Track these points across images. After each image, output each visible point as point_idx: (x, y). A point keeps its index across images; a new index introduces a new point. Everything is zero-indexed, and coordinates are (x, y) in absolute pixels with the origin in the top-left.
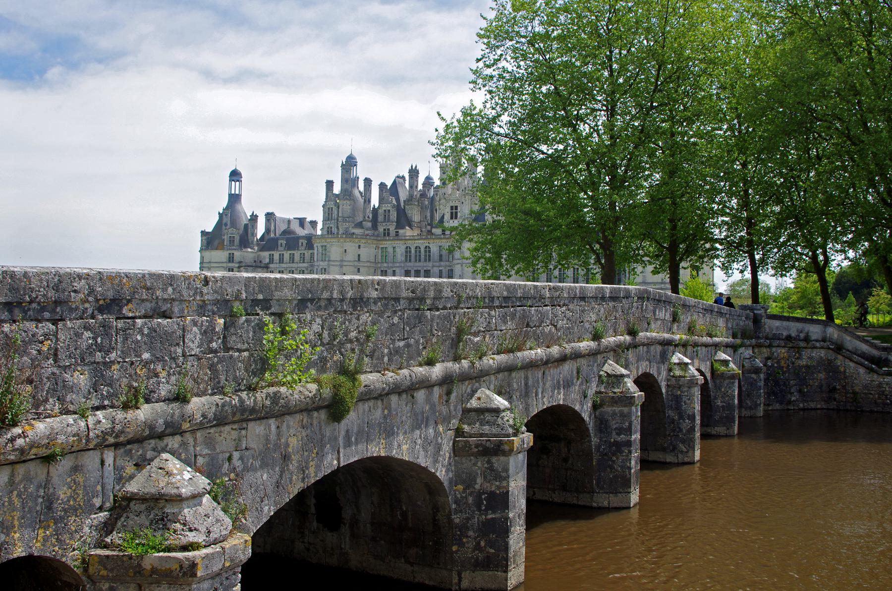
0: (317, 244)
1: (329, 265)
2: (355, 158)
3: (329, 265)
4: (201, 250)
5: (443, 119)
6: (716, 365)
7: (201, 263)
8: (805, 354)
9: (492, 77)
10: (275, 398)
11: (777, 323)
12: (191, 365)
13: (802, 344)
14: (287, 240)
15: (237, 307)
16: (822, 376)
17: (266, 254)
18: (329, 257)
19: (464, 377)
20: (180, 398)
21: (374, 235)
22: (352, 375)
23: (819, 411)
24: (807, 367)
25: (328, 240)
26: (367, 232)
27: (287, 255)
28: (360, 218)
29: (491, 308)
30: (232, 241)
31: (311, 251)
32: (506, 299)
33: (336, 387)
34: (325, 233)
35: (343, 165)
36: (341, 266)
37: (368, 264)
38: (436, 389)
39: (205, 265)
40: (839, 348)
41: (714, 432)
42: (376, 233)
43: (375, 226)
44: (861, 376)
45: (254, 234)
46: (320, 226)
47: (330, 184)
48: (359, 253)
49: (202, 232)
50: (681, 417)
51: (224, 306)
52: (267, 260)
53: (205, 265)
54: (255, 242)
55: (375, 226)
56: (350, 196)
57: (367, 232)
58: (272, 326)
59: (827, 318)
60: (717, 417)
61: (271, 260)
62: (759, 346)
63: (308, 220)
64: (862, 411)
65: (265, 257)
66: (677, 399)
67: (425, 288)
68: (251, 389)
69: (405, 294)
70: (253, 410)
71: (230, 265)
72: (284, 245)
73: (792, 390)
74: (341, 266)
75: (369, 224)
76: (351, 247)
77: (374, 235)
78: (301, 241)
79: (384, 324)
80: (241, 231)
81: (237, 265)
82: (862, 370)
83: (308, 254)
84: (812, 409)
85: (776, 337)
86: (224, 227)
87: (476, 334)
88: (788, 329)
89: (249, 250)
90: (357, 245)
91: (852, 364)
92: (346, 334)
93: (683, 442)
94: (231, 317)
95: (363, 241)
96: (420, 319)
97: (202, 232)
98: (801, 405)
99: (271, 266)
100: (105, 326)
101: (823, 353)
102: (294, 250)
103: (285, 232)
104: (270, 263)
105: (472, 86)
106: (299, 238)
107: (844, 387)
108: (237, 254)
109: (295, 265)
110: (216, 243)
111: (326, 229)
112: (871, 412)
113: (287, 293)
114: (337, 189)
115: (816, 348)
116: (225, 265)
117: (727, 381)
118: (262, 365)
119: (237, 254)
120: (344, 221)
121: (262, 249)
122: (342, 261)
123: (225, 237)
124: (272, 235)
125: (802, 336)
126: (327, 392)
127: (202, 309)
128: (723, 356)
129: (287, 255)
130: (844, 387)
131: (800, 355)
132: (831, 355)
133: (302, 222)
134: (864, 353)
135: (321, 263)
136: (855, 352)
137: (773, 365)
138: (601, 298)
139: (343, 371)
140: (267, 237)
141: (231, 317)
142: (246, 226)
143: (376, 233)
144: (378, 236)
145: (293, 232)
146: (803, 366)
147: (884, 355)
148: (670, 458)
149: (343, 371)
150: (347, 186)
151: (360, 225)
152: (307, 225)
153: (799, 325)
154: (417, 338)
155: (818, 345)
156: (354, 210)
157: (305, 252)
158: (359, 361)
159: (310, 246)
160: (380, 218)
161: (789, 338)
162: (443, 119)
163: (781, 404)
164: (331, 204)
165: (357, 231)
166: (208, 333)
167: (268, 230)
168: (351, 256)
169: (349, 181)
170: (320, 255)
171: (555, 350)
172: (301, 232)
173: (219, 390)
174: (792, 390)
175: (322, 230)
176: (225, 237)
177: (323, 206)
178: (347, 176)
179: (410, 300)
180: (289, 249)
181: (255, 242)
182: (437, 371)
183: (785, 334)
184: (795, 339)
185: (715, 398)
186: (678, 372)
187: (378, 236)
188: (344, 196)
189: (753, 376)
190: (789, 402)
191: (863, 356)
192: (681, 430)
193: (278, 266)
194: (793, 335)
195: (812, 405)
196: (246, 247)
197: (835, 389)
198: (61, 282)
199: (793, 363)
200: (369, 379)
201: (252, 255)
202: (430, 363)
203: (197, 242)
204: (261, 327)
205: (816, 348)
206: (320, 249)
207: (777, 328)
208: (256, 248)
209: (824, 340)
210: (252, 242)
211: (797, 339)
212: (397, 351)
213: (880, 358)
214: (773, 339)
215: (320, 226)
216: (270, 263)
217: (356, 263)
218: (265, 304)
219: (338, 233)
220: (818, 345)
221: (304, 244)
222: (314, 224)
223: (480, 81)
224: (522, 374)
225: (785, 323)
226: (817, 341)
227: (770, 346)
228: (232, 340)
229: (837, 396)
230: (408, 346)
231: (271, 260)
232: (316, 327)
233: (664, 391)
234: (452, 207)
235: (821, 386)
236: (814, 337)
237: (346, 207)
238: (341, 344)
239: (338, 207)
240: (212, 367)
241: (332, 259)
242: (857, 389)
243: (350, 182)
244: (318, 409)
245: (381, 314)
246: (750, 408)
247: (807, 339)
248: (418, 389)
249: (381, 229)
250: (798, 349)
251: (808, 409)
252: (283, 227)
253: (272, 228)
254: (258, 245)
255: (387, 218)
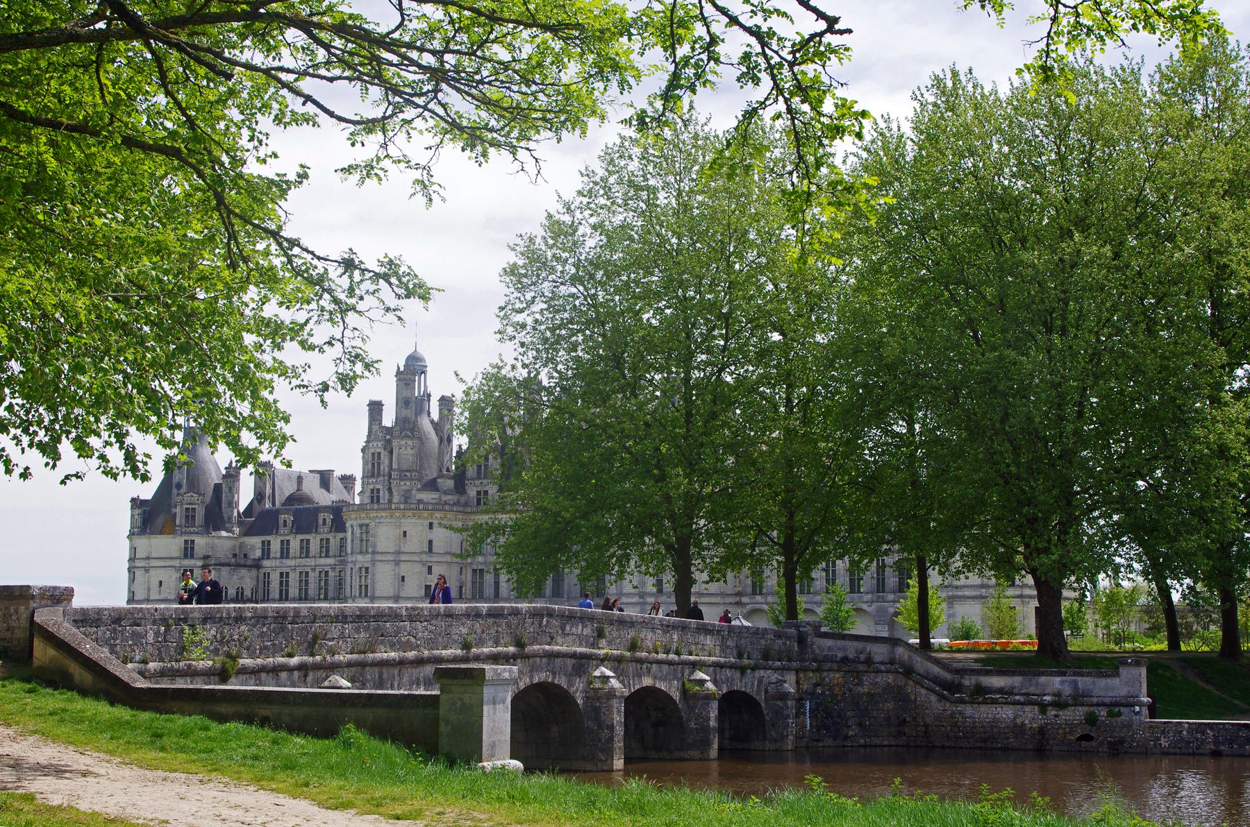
0: (351, 522)
1: (373, 562)
2: (420, 359)
3: (373, 562)
4: (131, 535)
5: (462, 380)
6: (688, 685)
7: (131, 560)
8: (867, 679)
9: (523, 326)
10: (189, 666)
11: (829, 643)
12: (150, 648)
13: (862, 668)
14: (297, 514)
15: (171, 621)
16: (890, 706)
17: (255, 541)
18: (374, 546)
19: (316, 667)
20: (145, 662)
21: (457, 503)
22: (234, 659)
23: (886, 749)
24: (869, 695)
25: (373, 514)
26: (444, 498)
27: (295, 544)
28: (431, 473)
29: (345, 623)
30: (190, 516)
31: (340, 535)
32: (358, 616)
33: (224, 664)
34: (367, 501)
35: (399, 373)
36: (397, 563)
37: (448, 558)
38: (296, 674)
39: (138, 564)
40: (908, 671)
41: (686, 756)
42: (463, 499)
43: (460, 487)
44: (933, 704)
45: (232, 504)
46: (358, 487)
47: (375, 408)
48: (430, 537)
49: (133, 500)
50: (600, 727)
51: (164, 621)
52: (258, 553)
53: (138, 564)
54: (235, 520)
55: (460, 487)
56: (412, 430)
57: (444, 498)
58: (187, 629)
59: (1170, 646)
60: (690, 741)
61: (266, 553)
62: (805, 670)
63: (338, 473)
64: (933, 747)
65: (253, 547)
66: (597, 711)
67: (286, 610)
68: (177, 661)
69: (271, 614)
70: (178, 671)
71: (188, 562)
72: (289, 523)
73: (849, 723)
74: (397, 563)
75: (450, 483)
76: (416, 528)
77: (457, 503)
78: (321, 516)
79: (256, 632)
80: (208, 499)
81: (200, 563)
82: (933, 698)
83: (334, 540)
84: (876, 746)
85: (826, 659)
86: (175, 491)
87: (330, 640)
88: (844, 649)
89: (224, 533)
90: (427, 523)
91: (923, 691)
92: (231, 636)
93: (602, 751)
94: (168, 627)
95: (438, 515)
96: (283, 629)
97: (133, 500)
98: (862, 741)
99: (266, 563)
100: (115, 629)
101: (890, 679)
102: (309, 532)
103: (291, 499)
104: (263, 558)
105: (499, 336)
106: (319, 509)
107: (914, 719)
108: (200, 542)
109: (311, 562)
110: (160, 520)
111: (368, 494)
112: (943, 747)
113: (196, 615)
114: (388, 419)
115: (881, 671)
116: (176, 563)
117: (700, 702)
118: (182, 649)
119: (200, 542)
120: (402, 478)
121: (249, 531)
122: (398, 553)
123: (178, 510)
124: (268, 505)
125: (862, 657)
126: (218, 665)
127: (154, 623)
128: (700, 675)
129: (295, 544)
130: (914, 719)
131: (860, 680)
132: (901, 681)
133: (325, 478)
134: (936, 677)
135: (360, 557)
136: (926, 676)
137: (823, 693)
138: (436, 615)
139: (229, 655)
140: (257, 509)
141: (168, 627)
142: (218, 488)
143: (463, 499)
144: (466, 505)
145: (308, 499)
146: (864, 694)
147: (957, 678)
148: (589, 767)
149: (229, 655)
150: (409, 413)
151: (432, 485)
152: (336, 484)
153: (859, 645)
154: (280, 640)
155: (883, 668)
156: (421, 454)
157: (330, 536)
158: (239, 651)
159: (339, 525)
160: (471, 471)
161: (845, 660)
162: (462, 380)
163: (835, 739)
164: (378, 446)
165: (427, 496)
166: (157, 634)
167: (259, 496)
168: (415, 543)
169: (411, 402)
170: (357, 541)
171: (411, 654)
172: (324, 498)
173: (162, 660)
174: (849, 723)
175: (361, 493)
176: (178, 510)
177: (363, 450)
178: (406, 393)
179: (275, 618)
180: (298, 532)
181: (235, 520)
182: (295, 661)
183: (840, 655)
184: (854, 661)
185: (689, 720)
186: (597, 685)
187: (466, 505)
188: (402, 431)
189: (779, 703)
190: (846, 737)
191: (936, 680)
192: (600, 740)
193: (278, 563)
194: (851, 656)
195: (877, 741)
196: (217, 529)
197: (904, 721)
198: (99, 611)
199: (850, 690)
200: (246, 661)
201: (229, 544)
202: (290, 655)
203: (124, 519)
204: (182, 631)
205: (881, 671)
206: (357, 531)
207: (830, 648)
208: (237, 530)
209: (892, 662)
210: (230, 518)
211: (856, 661)
212: (266, 648)
213: (953, 682)
214: (822, 663)
215: (358, 487)
216: (263, 558)
217: (425, 557)
218: (185, 620)
219: (390, 501)
220: (883, 668)
221: (329, 522)
222: (347, 480)
223: (510, 330)
224: (376, 669)
225: (840, 643)
226: (882, 663)
227: (818, 670)
228: (168, 637)
229: (907, 730)
230: (274, 645)
231: (266, 553)
232: (213, 632)
233: (580, 701)
234: (282, 574)
235: (888, 719)
236: (877, 658)
237: (405, 451)
238: (228, 642)
239: (391, 452)
240: (159, 649)
241: (379, 549)
242: (928, 720)
243: (412, 405)
244: (214, 675)
245: (254, 626)
246: (776, 740)
247: (869, 661)
248: (281, 671)
249: (472, 492)
250: (858, 674)
251: (871, 746)
252: (289, 489)
253: (268, 491)
254: (240, 524)
255: (483, 472)
